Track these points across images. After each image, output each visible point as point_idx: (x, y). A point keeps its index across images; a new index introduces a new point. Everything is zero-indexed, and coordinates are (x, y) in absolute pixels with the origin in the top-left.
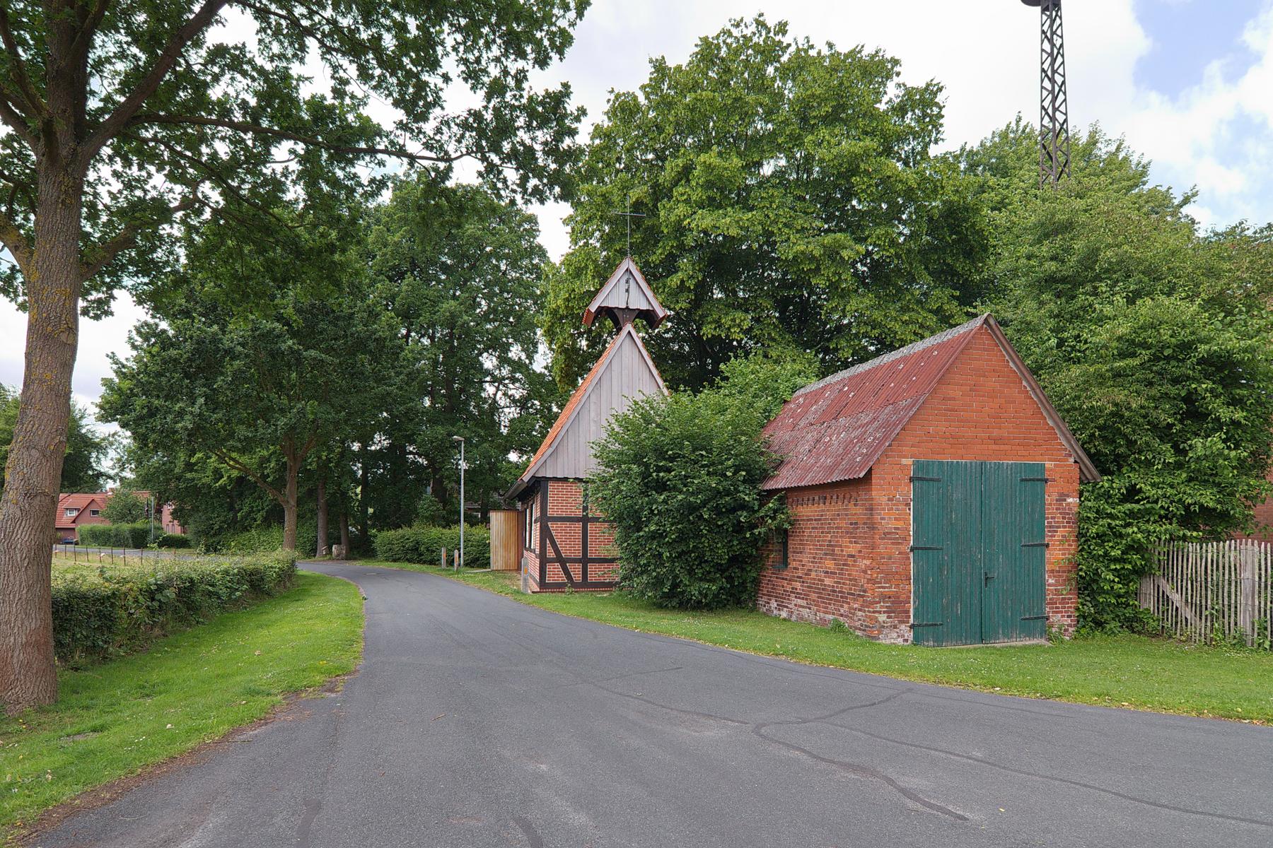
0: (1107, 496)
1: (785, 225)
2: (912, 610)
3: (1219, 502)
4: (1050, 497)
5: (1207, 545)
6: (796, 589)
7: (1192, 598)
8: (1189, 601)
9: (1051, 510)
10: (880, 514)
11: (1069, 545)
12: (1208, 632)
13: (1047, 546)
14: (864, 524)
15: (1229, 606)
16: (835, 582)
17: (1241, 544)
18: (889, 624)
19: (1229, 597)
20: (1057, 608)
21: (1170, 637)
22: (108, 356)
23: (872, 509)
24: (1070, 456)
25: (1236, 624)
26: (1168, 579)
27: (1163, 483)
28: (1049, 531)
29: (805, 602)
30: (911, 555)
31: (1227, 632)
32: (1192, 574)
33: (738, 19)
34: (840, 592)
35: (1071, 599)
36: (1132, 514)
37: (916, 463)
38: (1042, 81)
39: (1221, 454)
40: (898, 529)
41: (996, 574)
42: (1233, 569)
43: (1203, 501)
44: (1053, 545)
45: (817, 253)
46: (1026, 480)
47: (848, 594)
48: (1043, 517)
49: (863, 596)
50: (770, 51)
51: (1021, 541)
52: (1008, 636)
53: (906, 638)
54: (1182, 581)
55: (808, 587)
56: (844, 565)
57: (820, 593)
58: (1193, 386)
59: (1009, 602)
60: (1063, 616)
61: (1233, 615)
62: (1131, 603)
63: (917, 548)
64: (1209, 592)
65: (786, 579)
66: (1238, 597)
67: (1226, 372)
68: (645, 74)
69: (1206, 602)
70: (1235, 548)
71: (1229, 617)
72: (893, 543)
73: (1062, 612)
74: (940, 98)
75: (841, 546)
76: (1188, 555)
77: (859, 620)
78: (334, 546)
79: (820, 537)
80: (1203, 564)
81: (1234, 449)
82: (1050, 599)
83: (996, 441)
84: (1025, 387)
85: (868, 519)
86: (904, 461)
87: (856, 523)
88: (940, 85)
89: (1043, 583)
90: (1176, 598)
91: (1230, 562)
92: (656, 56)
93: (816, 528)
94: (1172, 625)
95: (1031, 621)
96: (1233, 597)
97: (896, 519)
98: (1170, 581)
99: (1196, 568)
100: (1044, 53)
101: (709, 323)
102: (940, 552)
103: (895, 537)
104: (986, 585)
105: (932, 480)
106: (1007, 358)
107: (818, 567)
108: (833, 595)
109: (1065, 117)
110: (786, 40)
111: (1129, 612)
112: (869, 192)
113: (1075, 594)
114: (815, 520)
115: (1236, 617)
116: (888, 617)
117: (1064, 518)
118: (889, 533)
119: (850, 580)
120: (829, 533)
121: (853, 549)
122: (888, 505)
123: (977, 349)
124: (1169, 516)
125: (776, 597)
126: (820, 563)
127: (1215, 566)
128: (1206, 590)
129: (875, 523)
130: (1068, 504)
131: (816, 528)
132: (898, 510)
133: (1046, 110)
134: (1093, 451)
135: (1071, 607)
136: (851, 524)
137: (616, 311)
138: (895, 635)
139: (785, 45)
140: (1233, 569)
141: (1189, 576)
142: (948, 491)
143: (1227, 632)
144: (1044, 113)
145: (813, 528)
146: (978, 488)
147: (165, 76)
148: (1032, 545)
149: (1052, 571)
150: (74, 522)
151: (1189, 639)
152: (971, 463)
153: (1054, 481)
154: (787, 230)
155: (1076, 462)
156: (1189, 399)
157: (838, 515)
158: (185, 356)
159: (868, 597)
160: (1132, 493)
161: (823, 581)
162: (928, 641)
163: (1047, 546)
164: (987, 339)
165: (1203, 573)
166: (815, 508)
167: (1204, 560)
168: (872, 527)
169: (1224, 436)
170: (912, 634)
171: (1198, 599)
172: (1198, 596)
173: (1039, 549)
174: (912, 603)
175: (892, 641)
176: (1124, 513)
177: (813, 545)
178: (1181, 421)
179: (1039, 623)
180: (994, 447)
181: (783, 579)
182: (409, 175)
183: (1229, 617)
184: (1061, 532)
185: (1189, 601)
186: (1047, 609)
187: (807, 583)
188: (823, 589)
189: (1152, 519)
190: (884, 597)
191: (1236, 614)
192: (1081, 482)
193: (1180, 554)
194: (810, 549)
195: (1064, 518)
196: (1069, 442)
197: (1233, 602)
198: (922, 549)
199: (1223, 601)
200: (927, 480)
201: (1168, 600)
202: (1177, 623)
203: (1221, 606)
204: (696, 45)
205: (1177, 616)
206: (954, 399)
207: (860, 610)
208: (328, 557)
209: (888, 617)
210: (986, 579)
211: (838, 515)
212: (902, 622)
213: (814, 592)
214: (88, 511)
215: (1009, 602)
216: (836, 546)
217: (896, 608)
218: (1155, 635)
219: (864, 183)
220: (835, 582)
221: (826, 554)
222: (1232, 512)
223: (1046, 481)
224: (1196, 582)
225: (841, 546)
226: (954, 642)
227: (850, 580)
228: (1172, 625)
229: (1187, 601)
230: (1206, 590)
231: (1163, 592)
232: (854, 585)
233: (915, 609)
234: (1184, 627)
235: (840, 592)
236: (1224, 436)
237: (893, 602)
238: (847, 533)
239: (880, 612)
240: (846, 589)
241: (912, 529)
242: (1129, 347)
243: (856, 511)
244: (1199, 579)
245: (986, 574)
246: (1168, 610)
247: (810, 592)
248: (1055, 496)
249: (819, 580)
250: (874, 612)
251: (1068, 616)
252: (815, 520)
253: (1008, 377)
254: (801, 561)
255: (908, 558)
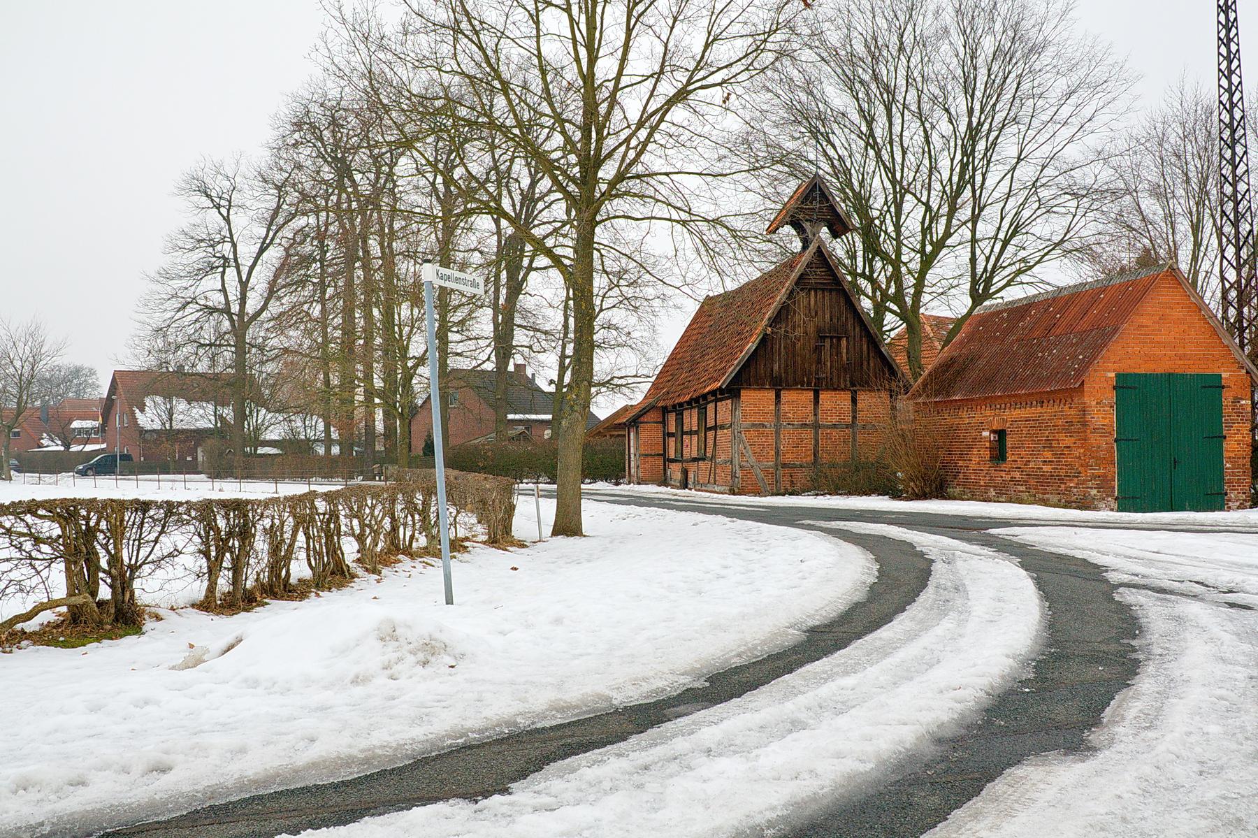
16: (1053, 469)
29: (1024, 487)
34: (1057, 476)
38: (1219, 48)
46: (1205, 387)
49: (1077, 477)
55: (1027, 475)
56: (1060, 454)
60: (1239, 493)
65: (1005, 471)
75: (1058, 440)
87: (1071, 422)
97: (1102, 418)
100: (1221, 89)
103: (1103, 431)
104: (1175, 468)
108: (1051, 479)
109: (1239, 80)
116: (1098, 492)
117: (1238, 416)
120: (1047, 430)
121: (1069, 441)
132: (1104, 411)
133: (1223, 72)
136: (1067, 422)
144: (1220, 42)
153: (1229, 387)
157: (1055, 416)
163: (1225, 437)
164: (1172, 280)
168: (1085, 424)
188: (1042, 475)
190: (1094, 477)
206: (1147, 326)
207: (1075, 488)
209: (1098, 492)
211: (1055, 416)
212: (1108, 496)
213: (1033, 478)
220: (1053, 469)
221: (1044, 447)
223: (1223, 387)
225: (1058, 440)
235: (1057, 476)
239: (1092, 488)
249: (1038, 468)
250: (1088, 488)
251: (1243, 493)
253: (1189, 308)
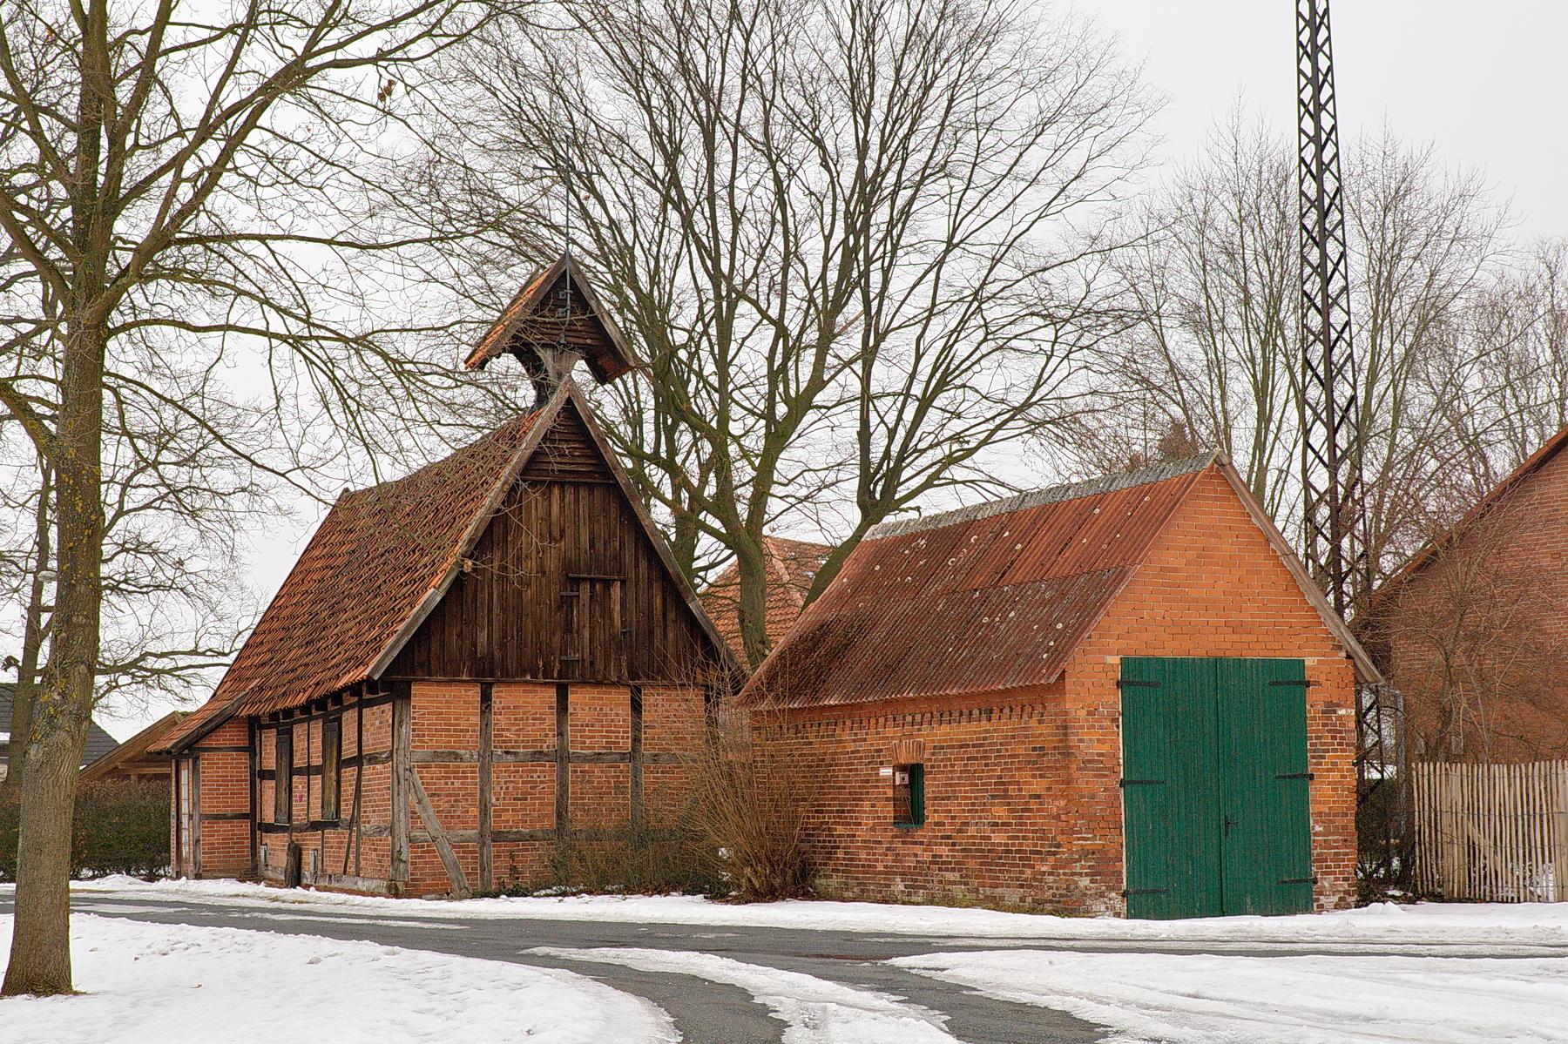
5: (1527, 767)
6: (941, 857)
9: (1314, 726)
11: (1342, 777)
14: (1055, 748)
18: (1093, 891)
20: (1327, 867)
23: (1066, 728)
28: (1313, 757)
35: (1347, 854)
44: (1320, 776)
46: (1277, 683)
47: (1032, 852)
49: (1054, 853)
57: (984, 857)
60: (1337, 879)
63: (1131, 782)
65: (922, 843)
72: (1096, 776)
73: (1335, 873)
75: (1018, 783)
77: (1050, 888)
79: (983, 771)
85: (1061, 741)
87: (1042, 749)
93: (976, 758)
97: (1099, 741)
107: (980, 818)
114: (974, 746)
116: (1092, 881)
118: (1089, 761)
119: (1034, 832)
121: (1038, 786)
123: (1206, 498)
125: (904, 874)
126: (982, 811)
129: (1071, 747)
131: (976, 758)
132: (1101, 728)
135: (1347, 866)
136: (1034, 749)
145: (969, 759)
147: (737, 516)
149: (1320, 814)
159: (1064, 853)
161: (989, 838)
163: (1311, 777)
164: (1220, 484)
166: (973, 726)
168: (1067, 753)
177: (971, 785)
180: (1236, 637)
181: (916, 843)
186: (1314, 869)
187: (960, 844)
188: (989, 851)
190: (1085, 854)
194: (966, 792)
195: (1334, 738)
207: (1051, 874)
209: (1092, 881)
216: (1010, 783)
221: (994, 797)
223: (1308, 684)
227: (1034, 832)
232: (1042, 839)
235: (1018, 852)
238: (1029, 763)
239: (1080, 874)
240: (1027, 846)
243: (1042, 730)
247: (967, 857)
252: (974, 746)
253: (1250, 536)
254: (950, 811)
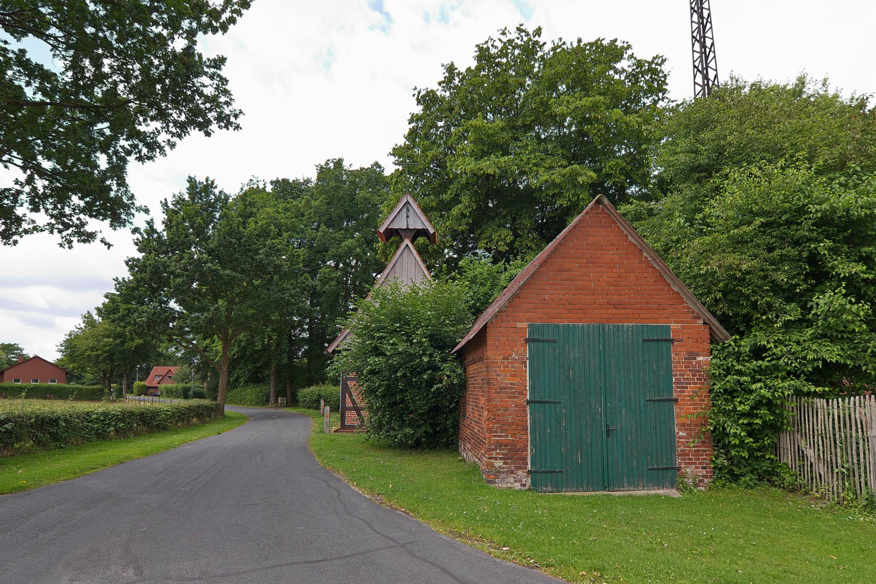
0: (738, 356)
1: (535, 165)
2: (529, 457)
3: (849, 357)
4: (677, 356)
7: (824, 456)
8: (822, 457)
10: (495, 371)
12: (840, 491)
13: (676, 400)
15: (859, 464)
17: (865, 401)
19: (858, 455)
21: (806, 493)
22: (114, 279)
24: (699, 318)
25: (866, 484)
26: (802, 434)
27: (790, 340)
28: (678, 387)
30: (528, 408)
31: (858, 492)
32: (822, 430)
33: (503, 28)
35: (706, 451)
36: (761, 371)
37: (530, 326)
39: (843, 310)
40: (514, 384)
41: (619, 427)
42: (859, 426)
43: (826, 356)
45: (558, 181)
46: (648, 341)
48: (669, 375)
50: (530, 49)
51: (645, 396)
52: (635, 485)
53: (524, 482)
54: (814, 437)
58: (813, 246)
59: (635, 453)
61: (863, 475)
62: (767, 457)
64: (838, 450)
66: (867, 456)
67: (849, 232)
68: (441, 75)
69: (836, 459)
70: (860, 403)
71: (860, 476)
72: (508, 397)
73: (695, 463)
74: (665, 68)
76: (817, 412)
78: (279, 398)
80: (831, 420)
81: (855, 303)
82: (682, 451)
83: (616, 306)
84: (646, 258)
86: (519, 325)
88: (663, 58)
89: (672, 436)
90: (810, 453)
91: (856, 419)
92: (447, 62)
94: (808, 480)
95: (660, 472)
96: (862, 456)
97: (511, 375)
98: (804, 437)
99: (825, 424)
101: (484, 239)
102: (558, 406)
105: (548, 341)
106: (625, 232)
110: (541, 40)
111: (766, 466)
112: (599, 135)
113: (710, 447)
115: (866, 477)
116: (504, 463)
122: (503, 363)
124: (798, 373)
127: (842, 423)
128: (836, 447)
129: (491, 379)
130: (699, 362)
132: (513, 367)
134: (719, 313)
135: (705, 459)
137: (399, 231)
138: (512, 480)
139: (541, 44)
140: (859, 426)
141: (820, 432)
142: (564, 350)
143: (858, 492)
146: (597, 348)
148: (658, 400)
149: (683, 425)
150: (159, 383)
151: (823, 497)
152: (588, 326)
154: (535, 168)
155: (705, 323)
156: (814, 259)
158: (148, 276)
160: (758, 352)
162: (546, 486)
164: (603, 218)
165: (831, 429)
167: (831, 417)
169: (844, 291)
170: (529, 479)
171: (829, 456)
172: (829, 453)
173: (666, 403)
174: (529, 451)
175: (509, 485)
176: (753, 370)
178: (805, 281)
179: (669, 473)
182: (328, 164)
183: (860, 476)
184: (690, 390)
185: (822, 457)
189: (780, 375)
190: (500, 445)
191: (865, 473)
192: (712, 342)
193: (810, 409)
196: (696, 305)
197: (862, 460)
198: (538, 402)
199: (852, 459)
200: (542, 341)
201: (803, 457)
202: (812, 478)
203: (850, 464)
204: (476, 52)
205: (811, 472)
206: (570, 270)
208: (275, 405)
209: (504, 463)
210: (608, 431)
214: (166, 377)
215: (635, 453)
217: (514, 455)
218: (793, 489)
219: (595, 129)
222: (864, 368)
224: (826, 438)
226: (575, 489)
228: (808, 480)
229: (819, 456)
230: (836, 447)
231: (798, 446)
233: (532, 456)
234: (819, 484)
236: (844, 291)
237: (509, 450)
239: (496, 459)
241: (528, 384)
242: (747, 214)
244: (828, 436)
245: (607, 426)
246: (804, 465)
248: (683, 355)
251: (703, 468)
255: (525, 411)
